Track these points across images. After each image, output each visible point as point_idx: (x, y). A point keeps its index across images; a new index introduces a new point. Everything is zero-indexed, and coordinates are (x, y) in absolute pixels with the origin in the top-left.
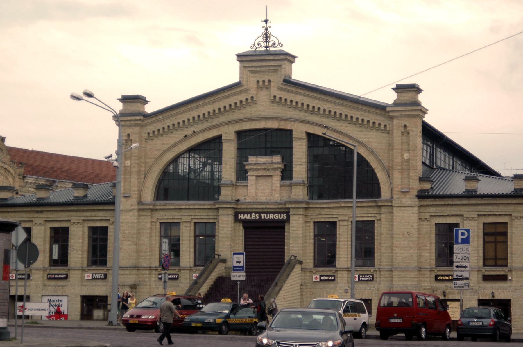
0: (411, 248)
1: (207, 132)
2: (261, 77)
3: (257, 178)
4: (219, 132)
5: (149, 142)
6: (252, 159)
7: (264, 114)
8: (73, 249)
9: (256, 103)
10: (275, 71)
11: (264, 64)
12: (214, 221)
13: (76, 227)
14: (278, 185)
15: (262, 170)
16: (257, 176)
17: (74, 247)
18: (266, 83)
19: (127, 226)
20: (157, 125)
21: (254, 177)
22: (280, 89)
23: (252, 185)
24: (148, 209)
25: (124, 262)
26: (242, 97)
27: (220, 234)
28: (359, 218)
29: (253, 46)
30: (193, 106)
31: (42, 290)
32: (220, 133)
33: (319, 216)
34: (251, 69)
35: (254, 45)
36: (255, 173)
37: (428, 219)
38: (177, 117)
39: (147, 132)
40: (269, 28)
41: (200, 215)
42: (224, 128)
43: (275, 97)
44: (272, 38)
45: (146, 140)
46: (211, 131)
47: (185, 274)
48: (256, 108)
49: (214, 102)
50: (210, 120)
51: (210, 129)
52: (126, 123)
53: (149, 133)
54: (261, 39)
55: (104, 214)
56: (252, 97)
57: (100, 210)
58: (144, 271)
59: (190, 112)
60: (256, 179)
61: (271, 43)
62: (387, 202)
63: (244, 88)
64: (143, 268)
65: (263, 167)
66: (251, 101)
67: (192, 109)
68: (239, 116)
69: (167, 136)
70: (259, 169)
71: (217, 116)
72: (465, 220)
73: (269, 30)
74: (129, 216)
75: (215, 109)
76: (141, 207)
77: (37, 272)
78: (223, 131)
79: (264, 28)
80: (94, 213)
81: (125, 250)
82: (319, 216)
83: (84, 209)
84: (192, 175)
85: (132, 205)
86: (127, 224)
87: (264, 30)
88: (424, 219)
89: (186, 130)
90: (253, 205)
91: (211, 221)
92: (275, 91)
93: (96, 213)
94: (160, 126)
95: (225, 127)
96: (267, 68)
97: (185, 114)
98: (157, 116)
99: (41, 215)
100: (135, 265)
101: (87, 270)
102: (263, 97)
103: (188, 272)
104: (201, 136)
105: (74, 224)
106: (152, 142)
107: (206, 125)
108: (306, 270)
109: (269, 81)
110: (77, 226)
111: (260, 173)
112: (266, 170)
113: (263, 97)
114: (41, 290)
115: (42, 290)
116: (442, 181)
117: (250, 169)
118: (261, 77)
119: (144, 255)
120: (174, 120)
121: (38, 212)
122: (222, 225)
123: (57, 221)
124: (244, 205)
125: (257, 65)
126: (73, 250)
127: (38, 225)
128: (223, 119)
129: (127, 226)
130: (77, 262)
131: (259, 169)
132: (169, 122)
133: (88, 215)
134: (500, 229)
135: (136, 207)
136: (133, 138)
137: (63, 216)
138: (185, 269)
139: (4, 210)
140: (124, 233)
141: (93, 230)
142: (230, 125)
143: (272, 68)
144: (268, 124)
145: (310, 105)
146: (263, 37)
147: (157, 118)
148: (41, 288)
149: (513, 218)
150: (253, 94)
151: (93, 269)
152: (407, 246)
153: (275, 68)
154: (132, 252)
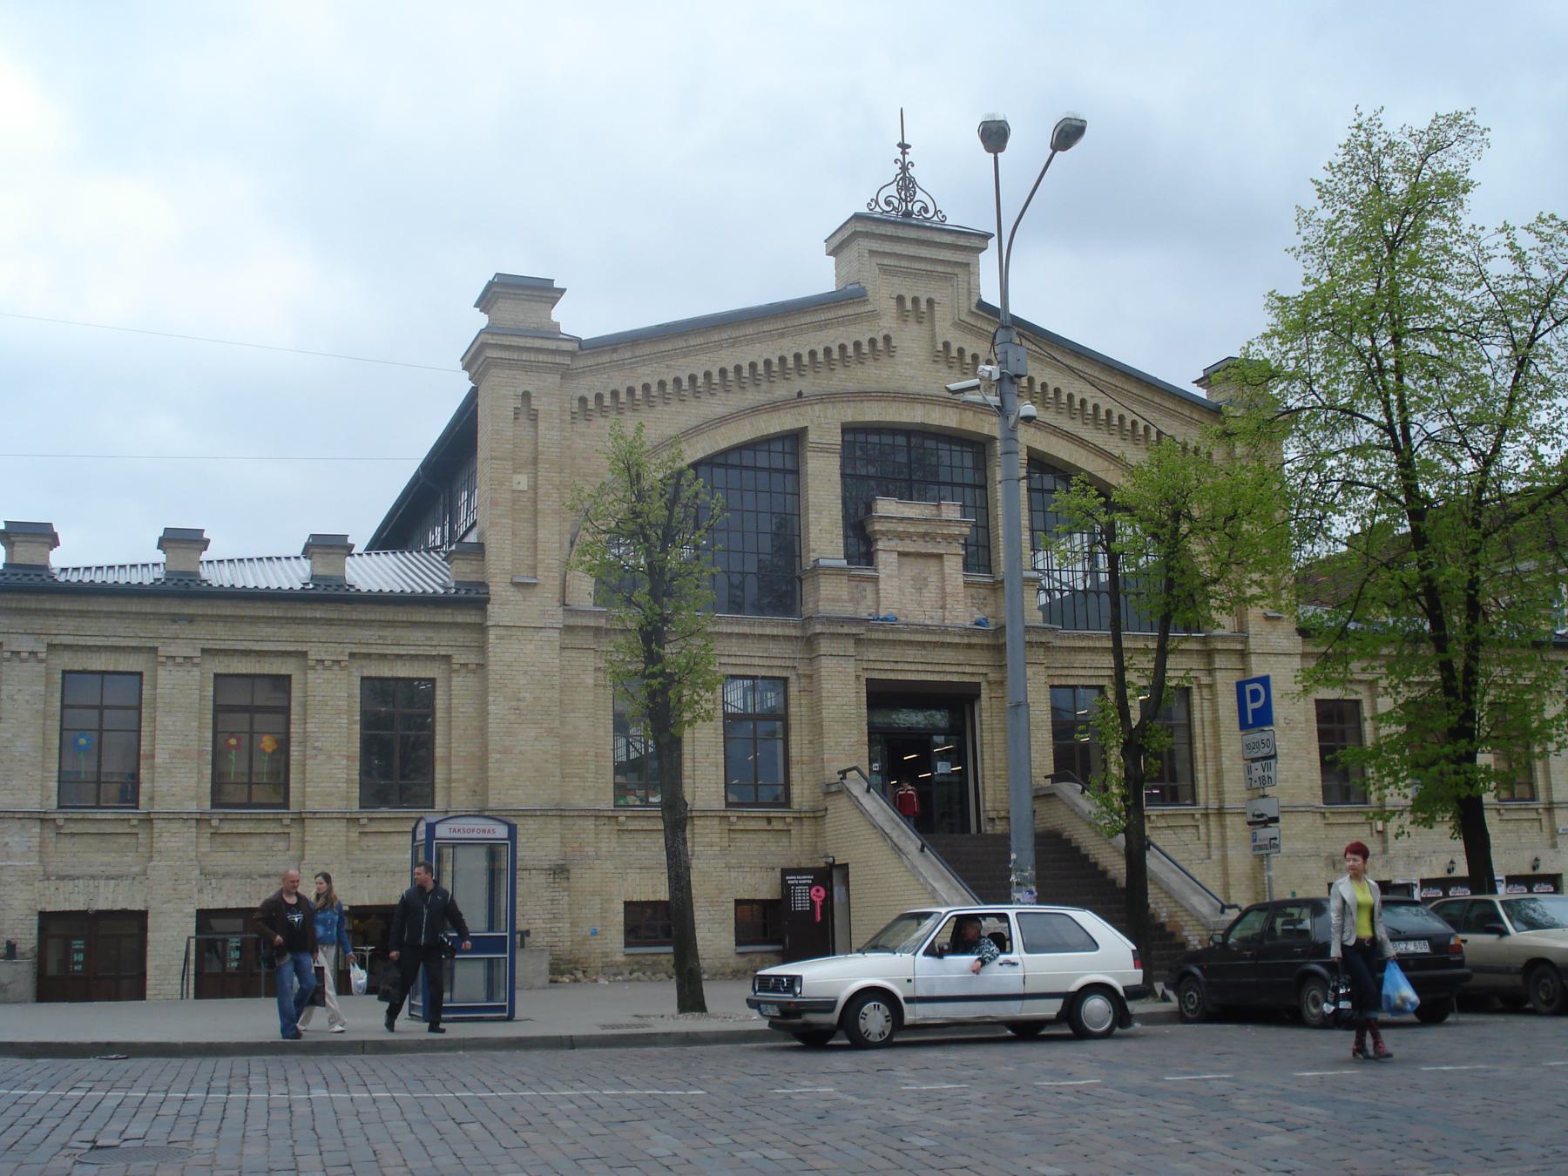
0: (1295, 758)
1: (765, 416)
2: (909, 289)
3: (904, 559)
4: (797, 420)
5: (581, 426)
6: (886, 506)
7: (913, 387)
8: (315, 748)
9: (892, 356)
10: (947, 277)
11: (924, 252)
12: (784, 674)
13: (328, 675)
14: (960, 581)
15: (915, 538)
16: (901, 554)
17: (316, 744)
18: (923, 306)
19: (528, 677)
20: (609, 378)
21: (895, 555)
22: (961, 325)
23: (889, 576)
24: (587, 628)
25: (520, 792)
26: (862, 334)
27: (824, 711)
28: (774, 670)
29: (873, 204)
30: (725, 336)
31: (201, 891)
32: (803, 424)
33: (1065, 672)
34: (887, 261)
35: (877, 203)
36: (896, 544)
37: (195, 660)
38: (672, 363)
39: (579, 394)
40: (910, 166)
41: (747, 654)
42: (813, 410)
43: (946, 345)
44: (919, 195)
45: (572, 418)
46: (775, 415)
47: (708, 831)
48: (891, 370)
49: (782, 335)
50: (764, 386)
51: (775, 407)
52: (525, 356)
53: (583, 400)
54: (892, 190)
55: (431, 639)
56: (887, 339)
57: (314, 621)
58: (580, 822)
59: (711, 355)
60: (899, 562)
61: (917, 207)
62: (1233, 641)
63: (870, 308)
64: (576, 813)
65: (921, 529)
66: (884, 348)
67: (719, 345)
68: (847, 384)
69: (637, 414)
70: (909, 535)
71: (787, 376)
72: (457, 671)
73: (912, 171)
74: (532, 647)
75: (784, 353)
76: (572, 622)
77: (175, 826)
78: (812, 421)
79: (899, 165)
80: (389, 634)
81: (521, 753)
82: (1065, 672)
83: (363, 617)
84: (1183, 552)
85: (544, 612)
86: (525, 673)
87: (897, 169)
88: (181, 660)
89: (695, 403)
90: (902, 631)
91: (776, 673)
92: (945, 331)
93: (399, 632)
94: (620, 382)
95: (816, 407)
96: (929, 267)
97: (698, 357)
98: (614, 350)
99: (186, 630)
100: (558, 804)
101: (365, 821)
102: (911, 340)
103: (714, 823)
104: (749, 427)
105: (319, 667)
106: (588, 427)
107: (752, 397)
108: (567, 814)
109: (930, 302)
110: (328, 672)
111: (910, 547)
112: (927, 539)
113: (911, 340)
114: (195, 890)
115: (201, 891)
116: (414, 573)
117: (883, 533)
118: (909, 289)
119: (577, 771)
120: (663, 370)
121: (175, 618)
122: (830, 686)
123: (246, 653)
124: (877, 631)
125: (904, 253)
126: (315, 752)
127: (179, 665)
128: (807, 384)
129: (528, 677)
130: (330, 794)
131: (909, 535)
132: (648, 375)
133: (224, 636)
134: (263, 697)
135: (558, 618)
136: (541, 408)
137: (417, 640)
138: (709, 814)
139: (41, 606)
140: (519, 700)
141: (375, 689)
142: (830, 405)
143: (940, 268)
144: (933, 416)
145: (1036, 379)
146: (898, 185)
147: (615, 357)
148: (194, 882)
149: (455, 667)
150: (890, 328)
151: (379, 816)
152: (1285, 751)
153: (949, 270)
154: (547, 761)
